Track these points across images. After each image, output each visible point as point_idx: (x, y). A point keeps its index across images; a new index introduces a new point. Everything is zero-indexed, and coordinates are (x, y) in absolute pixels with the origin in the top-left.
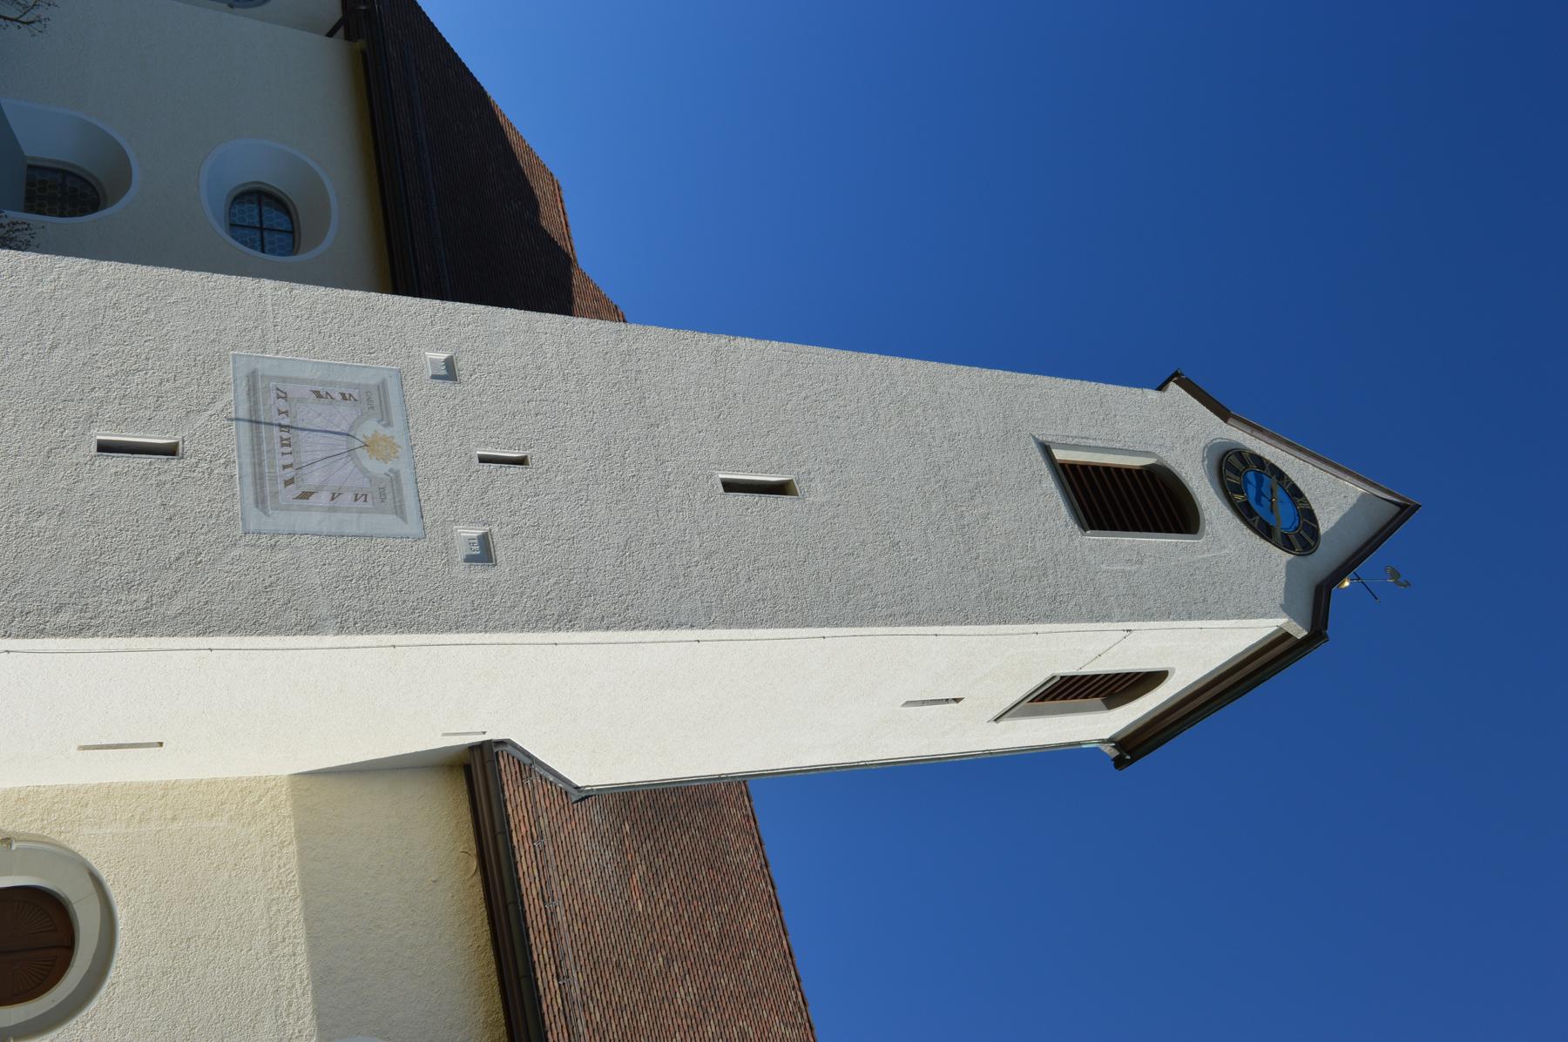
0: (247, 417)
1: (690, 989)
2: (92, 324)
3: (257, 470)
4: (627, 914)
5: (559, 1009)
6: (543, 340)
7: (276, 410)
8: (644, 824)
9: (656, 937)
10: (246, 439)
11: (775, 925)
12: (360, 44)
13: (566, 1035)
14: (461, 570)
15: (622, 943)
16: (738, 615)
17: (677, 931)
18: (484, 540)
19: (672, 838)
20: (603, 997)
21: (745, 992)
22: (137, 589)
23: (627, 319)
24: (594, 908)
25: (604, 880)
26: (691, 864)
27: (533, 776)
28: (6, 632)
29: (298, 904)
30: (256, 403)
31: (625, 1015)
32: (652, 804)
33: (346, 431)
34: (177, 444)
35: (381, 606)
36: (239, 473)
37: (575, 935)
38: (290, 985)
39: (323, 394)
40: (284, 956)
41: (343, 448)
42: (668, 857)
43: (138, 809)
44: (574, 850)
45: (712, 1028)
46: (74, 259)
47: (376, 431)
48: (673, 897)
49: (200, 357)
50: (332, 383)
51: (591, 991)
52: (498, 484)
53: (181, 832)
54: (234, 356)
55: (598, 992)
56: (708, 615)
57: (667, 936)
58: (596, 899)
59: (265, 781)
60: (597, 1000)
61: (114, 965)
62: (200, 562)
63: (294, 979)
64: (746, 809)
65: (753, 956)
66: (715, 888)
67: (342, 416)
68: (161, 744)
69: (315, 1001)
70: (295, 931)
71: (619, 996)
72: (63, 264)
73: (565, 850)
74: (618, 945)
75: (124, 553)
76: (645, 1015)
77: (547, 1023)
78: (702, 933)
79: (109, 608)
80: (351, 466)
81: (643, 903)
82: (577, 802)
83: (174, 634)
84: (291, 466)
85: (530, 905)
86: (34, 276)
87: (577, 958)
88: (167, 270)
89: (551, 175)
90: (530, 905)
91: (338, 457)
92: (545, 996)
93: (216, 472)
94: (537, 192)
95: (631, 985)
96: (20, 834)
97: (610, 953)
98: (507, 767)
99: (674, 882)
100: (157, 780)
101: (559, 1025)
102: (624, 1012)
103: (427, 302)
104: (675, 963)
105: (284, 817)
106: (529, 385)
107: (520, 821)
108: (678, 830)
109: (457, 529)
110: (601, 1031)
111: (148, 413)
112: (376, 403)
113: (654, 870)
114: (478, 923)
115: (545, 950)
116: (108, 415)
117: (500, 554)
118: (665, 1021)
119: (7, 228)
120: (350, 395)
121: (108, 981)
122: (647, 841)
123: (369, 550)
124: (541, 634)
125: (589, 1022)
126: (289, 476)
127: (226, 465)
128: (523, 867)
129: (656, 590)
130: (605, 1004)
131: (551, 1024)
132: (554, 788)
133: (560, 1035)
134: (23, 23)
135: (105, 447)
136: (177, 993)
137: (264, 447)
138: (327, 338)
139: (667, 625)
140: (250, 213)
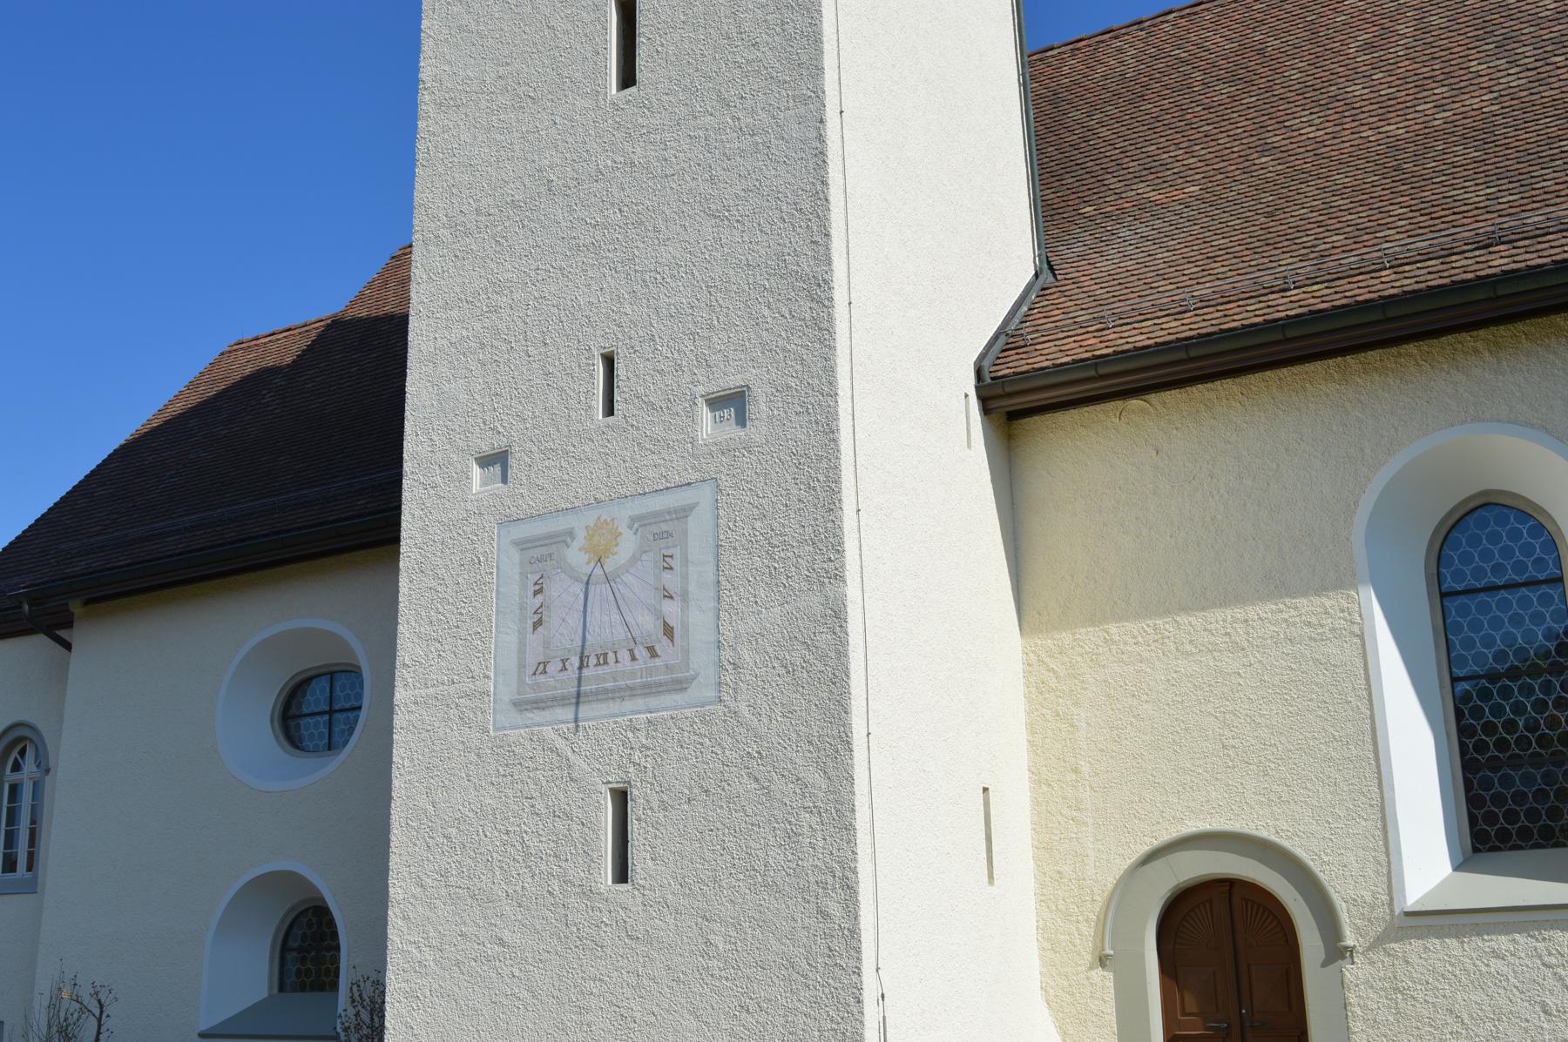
0: (573, 708)
1: (1304, 119)
2: (469, 901)
3: (639, 692)
4: (1204, 206)
5: (1327, 288)
6: (445, 342)
7: (562, 674)
8: (1085, 188)
9: (1234, 167)
10: (602, 708)
11: (1220, 9)
12: (76, 607)
13: (1361, 278)
14: (756, 431)
15: (1241, 210)
16: (805, 58)
17: (1227, 140)
18: (715, 403)
19: (1102, 150)
20: (1312, 232)
21: (1310, 47)
22: (796, 825)
23: (408, 243)
24: (1195, 248)
25: (1157, 236)
26: (1137, 124)
27: (1022, 332)
28: (854, 972)
29: (1183, 619)
30: (554, 699)
31: (1336, 204)
32: (1057, 178)
33: (582, 586)
34: (612, 790)
35: (807, 529)
36: (644, 713)
37: (1230, 270)
38: (1284, 625)
39: (536, 618)
40: (1248, 634)
41: (605, 588)
42: (1128, 154)
43: (1064, 812)
44: (1118, 276)
45: (1358, 90)
46: (390, 927)
47: (580, 549)
48: (1181, 146)
49: (501, 770)
50: (522, 607)
51: (1304, 248)
52: (641, 390)
53: (1093, 762)
54: (496, 729)
55: (1305, 239)
56: (805, 100)
57: (1233, 152)
58: (1182, 245)
59: (1029, 665)
60: (1316, 239)
61: (1255, 833)
62: (759, 753)
63: (1277, 620)
64: (1064, 53)
65: (1262, 37)
66: (1169, 91)
67: (562, 592)
68: (985, 790)
69: (1304, 594)
70: (1217, 622)
71: (1312, 212)
72: (397, 940)
73: (1118, 287)
74: (1244, 215)
75: (752, 844)
76: (1337, 177)
77: (1344, 301)
78: (1229, 106)
79: (821, 856)
80: (627, 578)
81: (1189, 184)
82: (1055, 276)
83: (851, 779)
84: (631, 651)
85: (1191, 329)
86: (415, 972)
87: (1260, 267)
88: (393, 817)
89: (222, 354)
90: (1191, 329)
91: (618, 597)
92: (1310, 305)
93: (644, 742)
94: (248, 371)
95: (1297, 197)
96: (1095, 945)
97: (1253, 225)
98: (1010, 365)
99: (1161, 145)
100: (1029, 794)
101: (1348, 287)
102: (1332, 204)
103: (406, 495)
104: (1269, 141)
105: (1075, 640)
106: (506, 356)
107: (1081, 346)
108: (1091, 143)
109: (703, 439)
110: (1357, 233)
111: (575, 827)
112: (544, 551)
113: (1145, 172)
114: (1212, 395)
115: (1248, 308)
116: (582, 874)
117: (733, 381)
118: (1346, 151)
119: (360, 1008)
120: (536, 584)
121: (1273, 838)
122: (1105, 182)
123: (735, 549)
124: (838, 322)
125: (1344, 248)
126: (645, 653)
127: (635, 730)
128: (1141, 340)
129: (773, 172)
130: (1321, 230)
131: (1346, 297)
132: (1037, 306)
133: (1360, 285)
134: (102, 1012)
135: (622, 874)
136: (1290, 758)
137: (609, 685)
138: (463, 618)
139: (821, 155)
140: (312, 728)
